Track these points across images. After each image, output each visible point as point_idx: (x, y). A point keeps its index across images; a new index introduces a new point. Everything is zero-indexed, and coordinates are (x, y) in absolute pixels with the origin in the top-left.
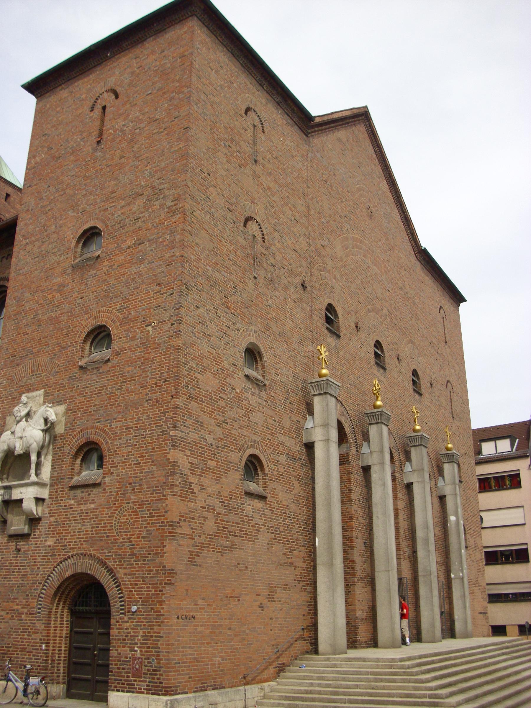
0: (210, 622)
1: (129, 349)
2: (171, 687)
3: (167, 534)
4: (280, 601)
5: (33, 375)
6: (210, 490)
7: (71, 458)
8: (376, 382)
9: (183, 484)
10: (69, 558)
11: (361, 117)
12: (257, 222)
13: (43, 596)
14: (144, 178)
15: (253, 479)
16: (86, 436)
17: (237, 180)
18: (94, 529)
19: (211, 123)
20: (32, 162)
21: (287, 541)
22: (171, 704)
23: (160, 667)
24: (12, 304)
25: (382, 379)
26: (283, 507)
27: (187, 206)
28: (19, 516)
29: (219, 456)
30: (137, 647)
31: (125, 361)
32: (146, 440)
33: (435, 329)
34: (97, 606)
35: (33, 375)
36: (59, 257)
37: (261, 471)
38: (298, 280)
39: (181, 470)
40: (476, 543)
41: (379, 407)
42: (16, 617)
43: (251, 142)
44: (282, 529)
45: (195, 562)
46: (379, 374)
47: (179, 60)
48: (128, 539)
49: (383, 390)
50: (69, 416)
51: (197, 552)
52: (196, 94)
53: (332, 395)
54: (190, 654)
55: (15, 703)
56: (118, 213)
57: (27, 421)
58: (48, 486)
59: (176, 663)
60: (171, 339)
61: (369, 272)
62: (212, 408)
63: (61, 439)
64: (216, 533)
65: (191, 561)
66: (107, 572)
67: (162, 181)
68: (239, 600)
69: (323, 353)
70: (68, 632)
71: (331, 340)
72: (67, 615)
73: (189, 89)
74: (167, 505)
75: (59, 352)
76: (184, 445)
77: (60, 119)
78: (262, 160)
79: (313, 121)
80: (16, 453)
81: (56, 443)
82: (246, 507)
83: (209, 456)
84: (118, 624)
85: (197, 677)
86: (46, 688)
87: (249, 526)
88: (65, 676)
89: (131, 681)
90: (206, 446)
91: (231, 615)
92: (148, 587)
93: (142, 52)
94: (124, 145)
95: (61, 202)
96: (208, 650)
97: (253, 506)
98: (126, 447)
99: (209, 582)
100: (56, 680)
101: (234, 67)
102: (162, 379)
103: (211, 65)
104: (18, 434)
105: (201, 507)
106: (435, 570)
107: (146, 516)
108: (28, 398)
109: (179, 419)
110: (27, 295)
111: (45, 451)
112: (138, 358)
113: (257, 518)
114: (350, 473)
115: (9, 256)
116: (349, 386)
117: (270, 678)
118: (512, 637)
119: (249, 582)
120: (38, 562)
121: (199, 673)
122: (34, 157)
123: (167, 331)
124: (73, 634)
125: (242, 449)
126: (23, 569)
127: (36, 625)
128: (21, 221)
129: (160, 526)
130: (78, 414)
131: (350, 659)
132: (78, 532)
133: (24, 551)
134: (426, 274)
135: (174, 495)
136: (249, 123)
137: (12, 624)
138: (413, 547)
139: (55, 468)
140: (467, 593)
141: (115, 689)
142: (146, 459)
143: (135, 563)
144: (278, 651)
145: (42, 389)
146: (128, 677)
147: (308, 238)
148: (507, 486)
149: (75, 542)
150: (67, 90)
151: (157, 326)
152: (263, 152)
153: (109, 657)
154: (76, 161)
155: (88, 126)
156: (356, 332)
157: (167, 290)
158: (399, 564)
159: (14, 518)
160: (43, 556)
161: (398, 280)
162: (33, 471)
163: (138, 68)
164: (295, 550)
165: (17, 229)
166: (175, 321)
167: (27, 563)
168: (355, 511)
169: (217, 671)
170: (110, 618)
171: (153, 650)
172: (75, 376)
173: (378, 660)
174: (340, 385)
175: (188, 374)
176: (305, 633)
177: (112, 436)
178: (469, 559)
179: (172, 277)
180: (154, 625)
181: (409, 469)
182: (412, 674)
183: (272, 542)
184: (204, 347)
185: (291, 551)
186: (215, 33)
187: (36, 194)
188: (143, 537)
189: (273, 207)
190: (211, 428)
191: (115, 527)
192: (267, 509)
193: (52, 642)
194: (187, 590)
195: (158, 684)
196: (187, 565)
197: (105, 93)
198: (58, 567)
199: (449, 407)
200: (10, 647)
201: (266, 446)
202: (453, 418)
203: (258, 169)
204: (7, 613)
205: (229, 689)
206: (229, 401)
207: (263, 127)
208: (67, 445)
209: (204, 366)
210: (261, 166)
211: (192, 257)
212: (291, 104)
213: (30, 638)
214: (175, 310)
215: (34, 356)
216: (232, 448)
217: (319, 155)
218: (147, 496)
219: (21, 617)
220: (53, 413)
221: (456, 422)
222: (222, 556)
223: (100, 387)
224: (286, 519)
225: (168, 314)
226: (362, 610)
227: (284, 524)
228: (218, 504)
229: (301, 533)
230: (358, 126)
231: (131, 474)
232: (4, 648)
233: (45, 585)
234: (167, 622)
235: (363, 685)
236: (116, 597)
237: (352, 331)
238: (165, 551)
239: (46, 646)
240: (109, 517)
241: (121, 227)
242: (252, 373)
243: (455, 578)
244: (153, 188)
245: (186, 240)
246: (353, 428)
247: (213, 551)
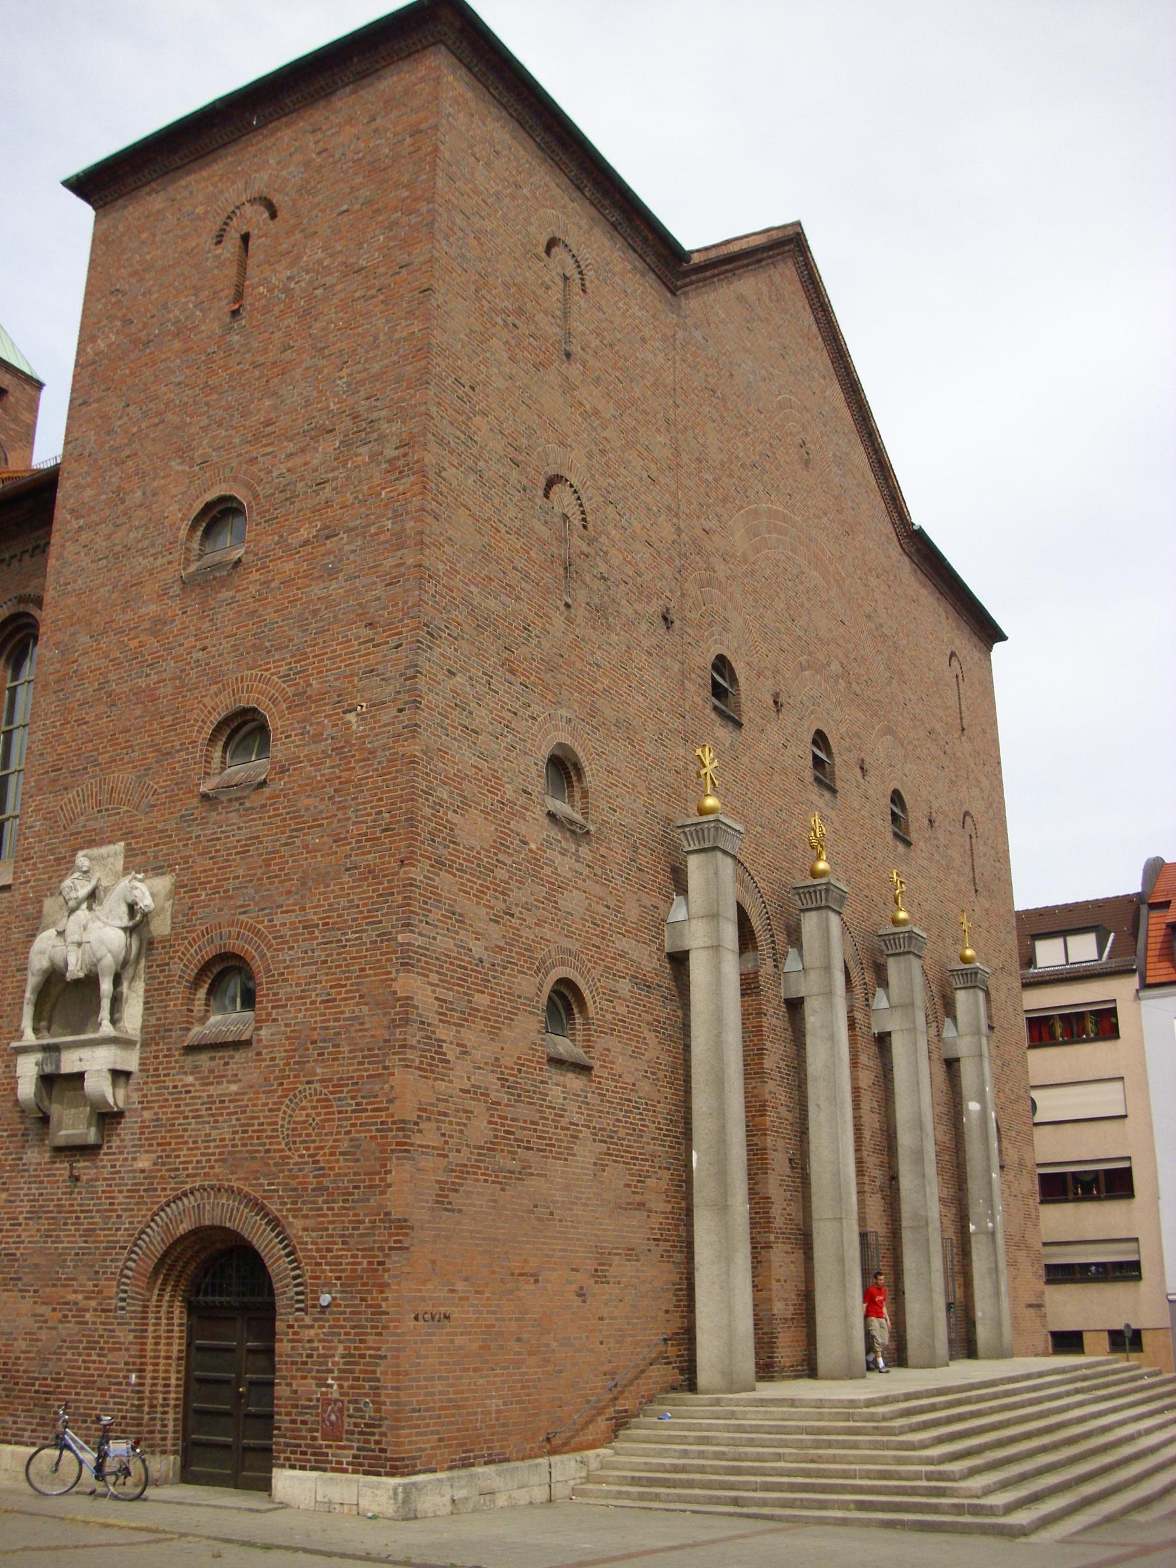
0: (480, 1326)
1: (309, 761)
2: (403, 1459)
3: (394, 1147)
4: (619, 1283)
5: (99, 811)
6: (478, 1054)
7: (185, 987)
8: (815, 821)
9: (425, 1044)
10: (186, 1195)
11: (788, 246)
12: (571, 486)
13: (130, 1273)
14: (337, 395)
15: (563, 1030)
16: (217, 942)
17: (530, 397)
18: (237, 1137)
19: (477, 277)
20: (88, 350)
21: (632, 1158)
22: (404, 1492)
23: (381, 1419)
24: (51, 658)
25: (828, 811)
26: (625, 1088)
27: (429, 459)
28: (77, 1107)
29: (496, 984)
30: (333, 1379)
31: (299, 786)
32: (348, 953)
33: (939, 702)
34: (244, 1294)
35: (99, 811)
36: (151, 559)
37: (580, 1012)
38: (656, 607)
39: (420, 1015)
40: (1021, 1159)
41: (823, 874)
42: (74, 1316)
43: (558, 313)
44: (622, 1133)
45: (450, 1203)
46: (820, 803)
47: (409, 140)
48: (310, 1156)
49: (831, 837)
50: (181, 899)
51: (453, 1183)
52: (445, 215)
53: (725, 852)
54: (441, 1393)
55: (78, 1493)
56: (279, 469)
57: (90, 908)
58: (138, 1046)
59: (414, 1410)
60: (397, 741)
61: (802, 583)
62: (481, 885)
63: (164, 947)
64: (492, 1143)
65: (442, 1203)
66: (267, 1224)
67: (375, 403)
68: (537, 1281)
69: (707, 762)
70: (184, 1348)
71: (723, 732)
72: (181, 1312)
73: (431, 206)
74: (392, 1087)
75: (157, 762)
76: (426, 963)
77: (148, 257)
78: (581, 352)
79: (688, 262)
80: (69, 976)
81: (152, 955)
82: (551, 1090)
83: (476, 984)
84: (291, 1331)
85: (456, 1438)
86: (143, 1461)
87: (556, 1127)
88: (177, 1439)
89: (320, 1447)
90: (470, 963)
91: (520, 1313)
92: (353, 1256)
93: (327, 118)
94: (291, 321)
95: (153, 440)
96: (475, 1384)
97: (564, 1087)
98: (303, 965)
99: (477, 1245)
100: (158, 1445)
101: (522, 152)
102: (380, 825)
103: (476, 149)
104: (73, 935)
105: (461, 1090)
106: (937, 1216)
107: (349, 1109)
108: (91, 859)
109: (417, 910)
110: (84, 639)
111: (129, 971)
112: (327, 780)
113: (572, 1112)
114: (760, 1014)
115: (42, 549)
116: (759, 829)
117: (599, 1440)
118: (1096, 1355)
119: (557, 1244)
120: (119, 1204)
121: (458, 1430)
122: (93, 339)
123: (389, 724)
124: (193, 1352)
125: (542, 968)
126: (85, 1218)
127: (117, 1333)
128: (68, 479)
129: (378, 1130)
130: (199, 896)
131: (762, 1402)
132: (203, 1141)
133: (88, 1181)
134: (921, 583)
135: (407, 1066)
136: (554, 273)
137: (64, 1332)
138: (890, 1168)
139: (152, 1008)
140: (1002, 1265)
141: (287, 1463)
142: (347, 992)
143: (325, 1206)
144: (616, 1386)
145: (121, 840)
146: (314, 1439)
147: (676, 515)
148: (1088, 1035)
149: (198, 1162)
150: (162, 193)
151: (367, 712)
152: (583, 333)
153: (273, 1398)
154: (186, 351)
155: (209, 275)
156: (774, 714)
157: (388, 636)
158: (861, 1203)
159: (65, 1112)
160: (129, 1191)
161: (863, 598)
162: (105, 1013)
163: (319, 153)
164: (649, 1177)
165: (59, 495)
166: (406, 703)
167: (94, 1205)
168: (771, 1093)
169: (493, 1426)
170: (273, 1319)
171: (366, 1384)
172: (192, 814)
173: (820, 1403)
174: (742, 830)
175: (433, 815)
176: (669, 1348)
177: (274, 942)
178: (1007, 1192)
179: (398, 611)
180: (367, 1334)
181: (884, 1004)
182: (891, 1432)
183: (603, 1159)
184: (464, 757)
185: (642, 1178)
186: (483, 79)
187: (99, 421)
188: (342, 1154)
189: (603, 452)
190: (480, 926)
191: (282, 1132)
192: (593, 1093)
193: (151, 1368)
194: (434, 1262)
195: (377, 1453)
196: (433, 1209)
197: (248, 205)
198: (162, 1214)
199: (967, 869)
200: (62, 1380)
201: (590, 961)
202: (976, 891)
203: (574, 371)
204: (54, 1310)
205: (518, 1464)
206: (516, 869)
207: (582, 279)
208: (176, 960)
209: (465, 797)
210: (578, 365)
211: (441, 566)
212: (642, 227)
213: (105, 1360)
214: (406, 680)
215: (101, 770)
216: (522, 966)
217: (698, 335)
218: (351, 1068)
219: (83, 1316)
220: (146, 892)
221: (982, 900)
222: (503, 1190)
223: (247, 839)
224: (631, 1112)
225: (389, 689)
226: (785, 1300)
227: (626, 1122)
228: (495, 1084)
229: (662, 1140)
230: (781, 267)
231: (315, 1022)
232: (49, 1381)
233: (134, 1252)
234: (396, 1327)
235: (790, 1454)
236: (286, 1277)
237: (766, 713)
238: (389, 1181)
239: (138, 1377)
240: (270, 1110)
241: (286, 499)
242: (561, 807)
243: (976, 1233)
244: (355, 417)
245: (427, 532)
246: (768, 918)
247: (486, 1181)
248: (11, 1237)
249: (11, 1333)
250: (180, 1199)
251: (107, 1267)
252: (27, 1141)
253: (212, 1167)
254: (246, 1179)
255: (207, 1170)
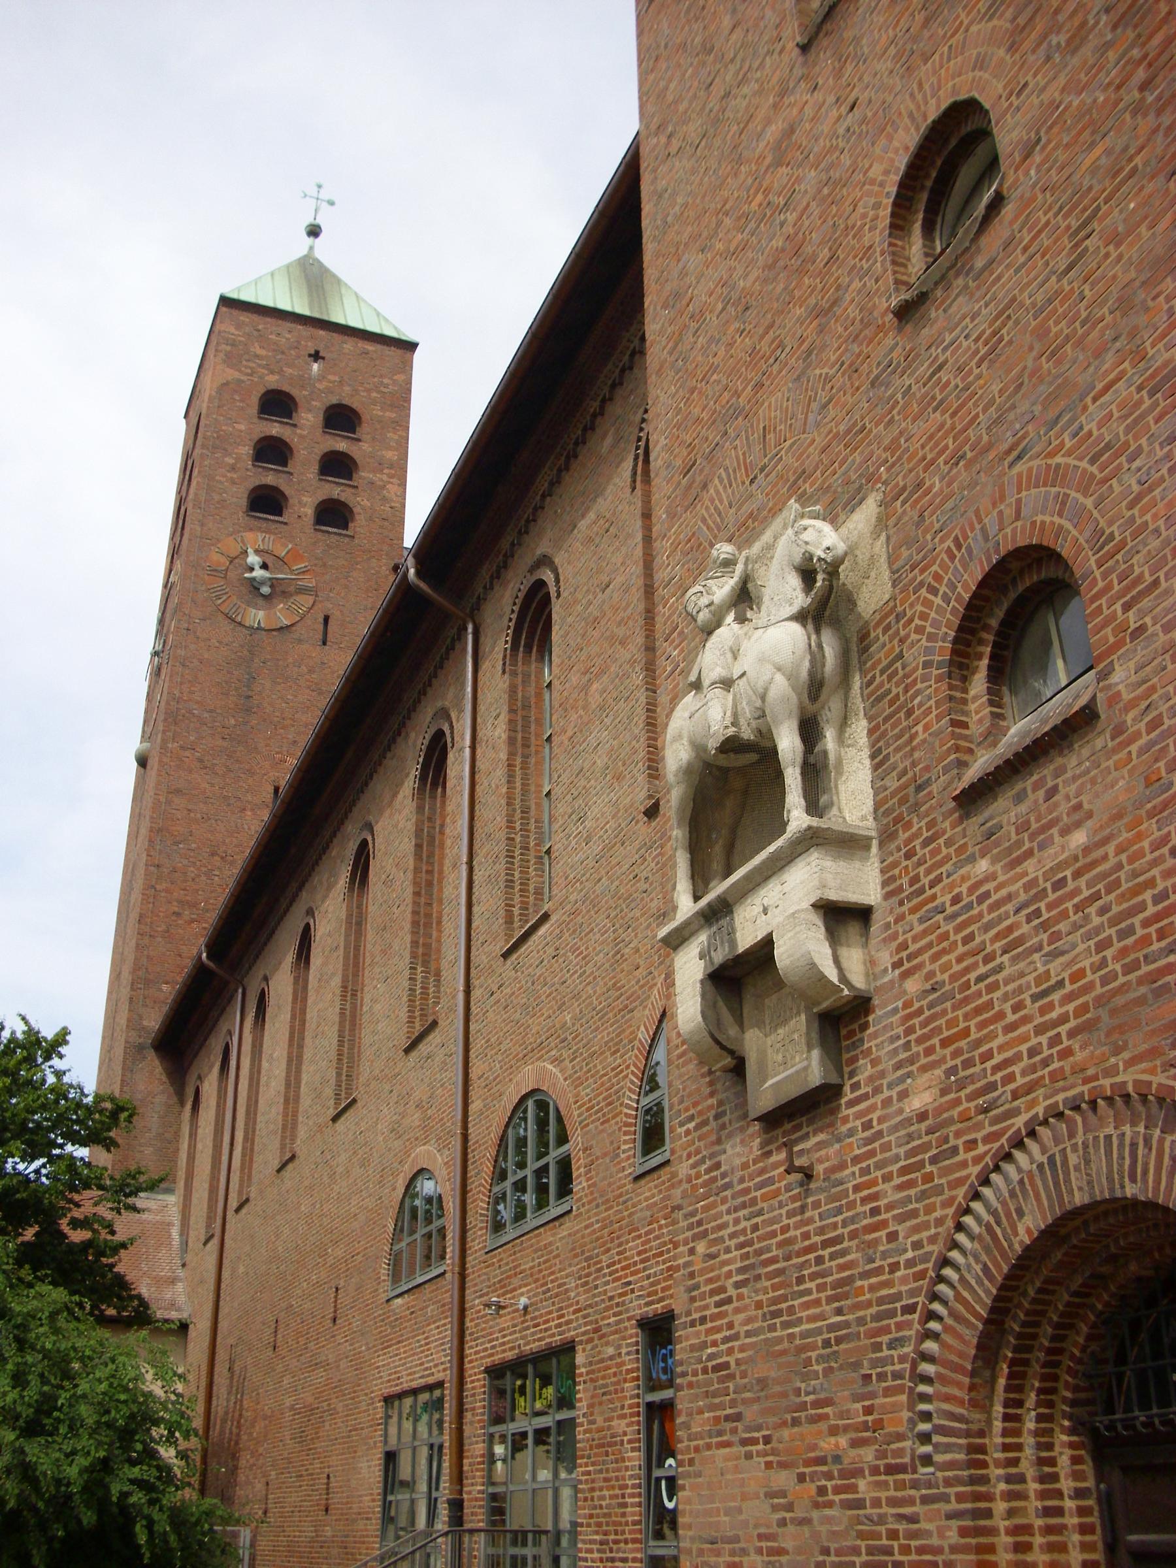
10: (1019, 1144)
18: (1109, 953)
42: (838, 1490)
57: (741, 619)
58: (874, 849)
72: (1075, 1460)
81: (871, 657)
127: (924, 1525)
137: (823, 1529)
167: (845, 1223)
177: (1094, 469)
198: (976, 1206)
233: (932, 1316)
248: (718, 1330)
249: (736, 1539)
250: (1008, 1157)
251: (884, 1362)
252: (723, 1127)
253: (1067, 1053)
254: (1153, 1053)
255: (1056, 1065)
